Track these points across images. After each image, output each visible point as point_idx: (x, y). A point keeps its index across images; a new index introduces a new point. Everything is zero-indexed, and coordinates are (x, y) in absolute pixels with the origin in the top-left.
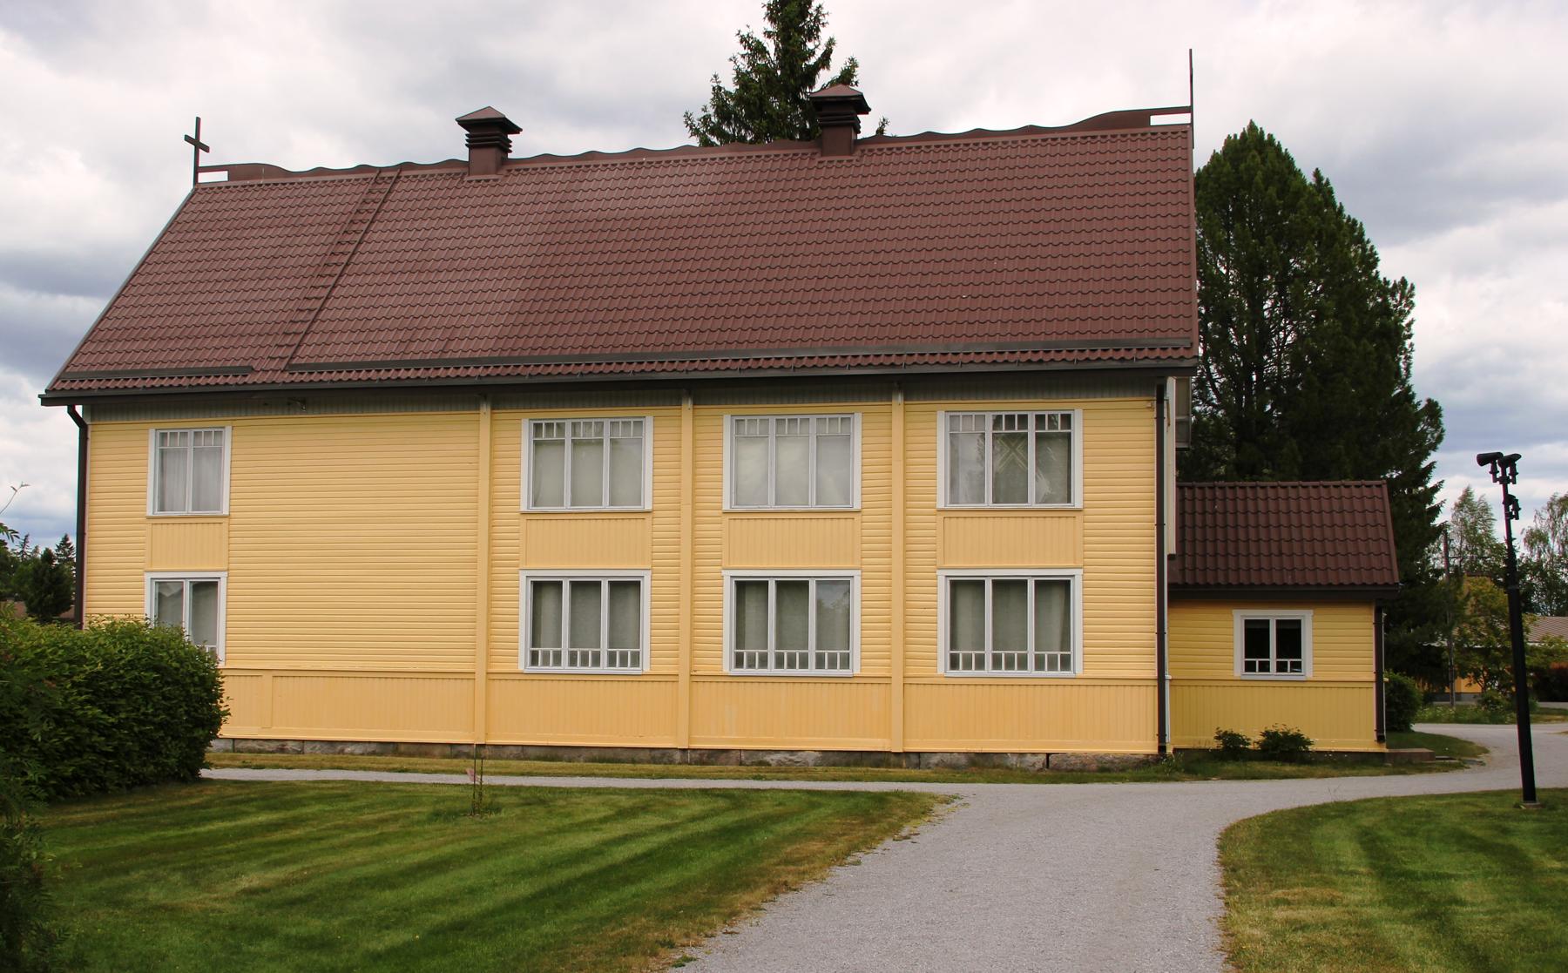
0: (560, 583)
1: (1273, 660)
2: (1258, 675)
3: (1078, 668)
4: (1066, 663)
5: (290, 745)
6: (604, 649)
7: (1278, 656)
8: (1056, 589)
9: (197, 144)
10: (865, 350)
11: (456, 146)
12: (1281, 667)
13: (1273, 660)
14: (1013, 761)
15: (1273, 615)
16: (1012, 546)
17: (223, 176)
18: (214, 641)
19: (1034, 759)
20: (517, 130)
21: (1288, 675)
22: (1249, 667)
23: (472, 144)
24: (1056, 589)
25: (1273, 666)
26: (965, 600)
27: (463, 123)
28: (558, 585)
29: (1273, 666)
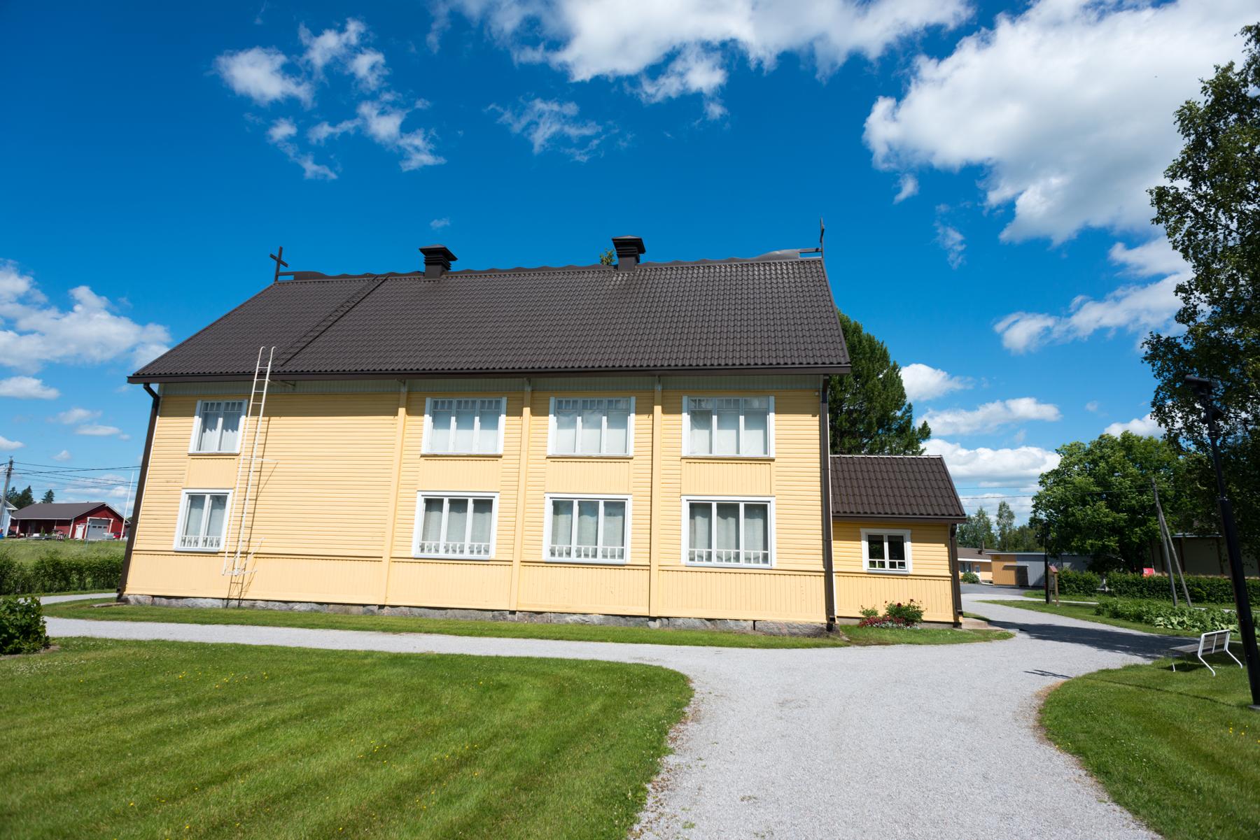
0: (442, 501)
1: (887, 560)
2: (877, 569)
3: (774, 562)
4: (765, 558)
5: (259, 603)
6: (574, 546)
7: (891, 558)
8: (758, 510)
9: (280, 262)
10: (463, 363)
11: (419, 263)
12: (892, 565)
13: (887, 560)
14: (732, 624)
15: (885, 532)
16: (738, 485)
17: (291, 278)
18: (220, 534)
19: (744, 624)
20: (454, 259)
21: (897, 570)
22: (872, 564)
23: (427, 263)
24: (758, 510)
25: (887, 565)
26: (700, 521)
27: (422, 251)
28: (708, 506)
29: (887, 565)
